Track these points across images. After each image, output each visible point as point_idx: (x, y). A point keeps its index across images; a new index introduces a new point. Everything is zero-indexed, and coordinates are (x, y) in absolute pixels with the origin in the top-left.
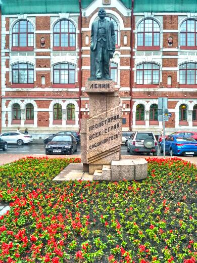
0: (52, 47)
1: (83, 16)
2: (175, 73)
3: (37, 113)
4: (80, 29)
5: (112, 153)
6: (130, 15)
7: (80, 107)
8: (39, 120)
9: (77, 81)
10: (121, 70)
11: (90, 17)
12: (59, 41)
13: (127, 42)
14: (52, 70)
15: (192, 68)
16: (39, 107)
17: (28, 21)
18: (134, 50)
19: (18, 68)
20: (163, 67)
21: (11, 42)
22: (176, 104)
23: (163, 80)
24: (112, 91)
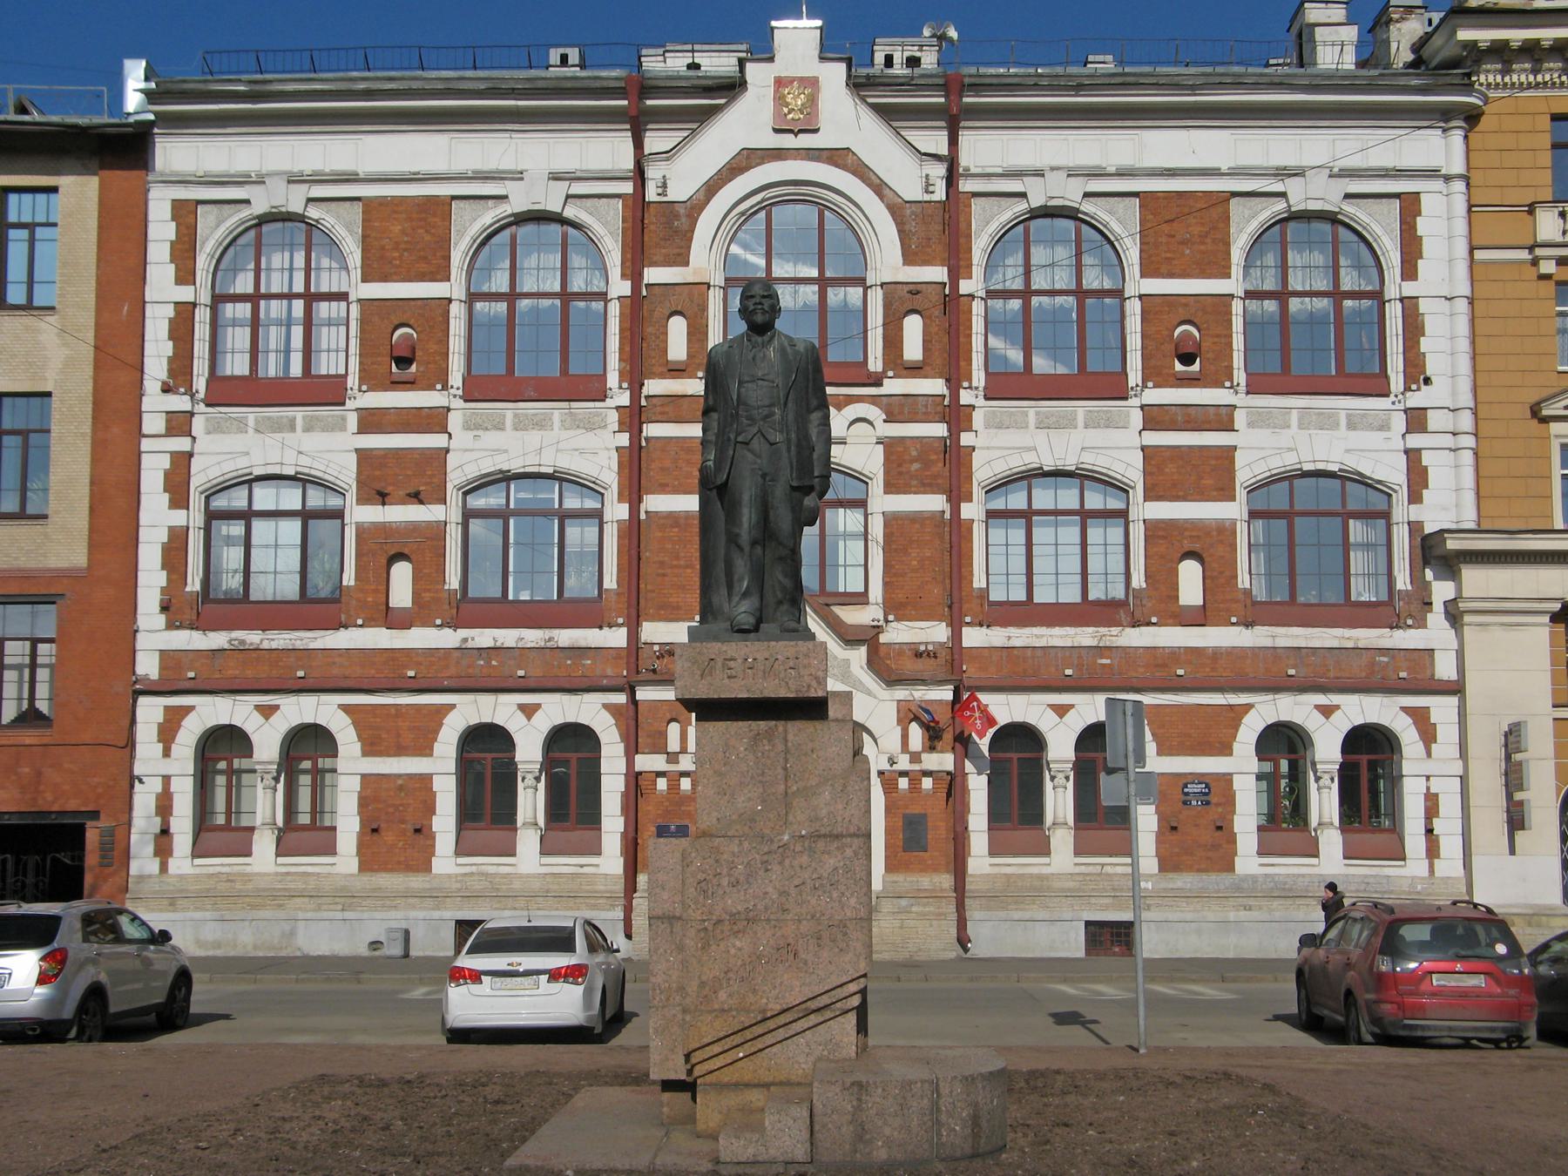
1: (652, 194)
2: (1224, 532)
4: (633, 272)
6: (940, 194)
7: (632, 749)
8: (371, 830)
9: (610, 582)
11: (696, 207)
13: (926, 349)
14: (455, 516)
15: (1323, 507)
16: (371, 747)
18: (966, 397)
19: (1023, 505)
21: (201, 348)
22: (1236, 726)
23: (1148, 576)
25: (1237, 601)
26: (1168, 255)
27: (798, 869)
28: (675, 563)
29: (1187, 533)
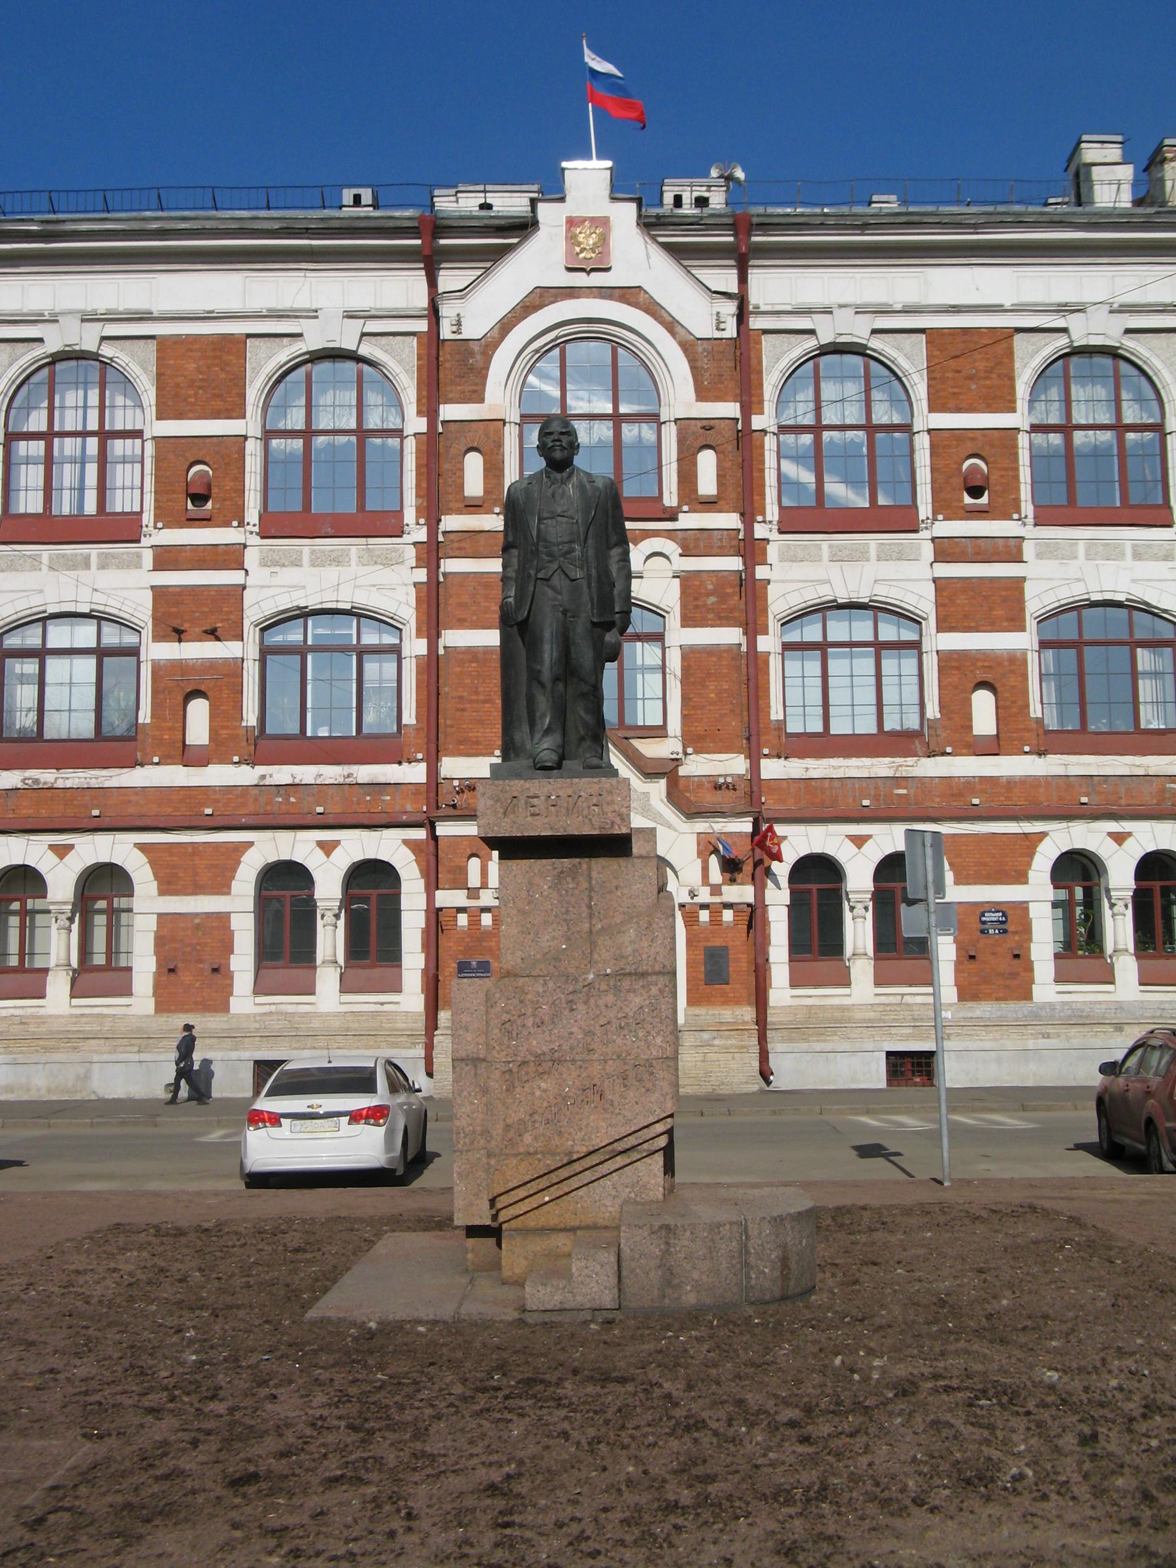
0: (252, 515)
1: (446, 332)
2: (1015, 662)
3: (151, 923)
4: (429, 409)
5: (620, 1161)
7: (433, 884)
8: (167, 970)
10: (690, 655)
12: (299, 483)
16: (168, 885)
17: (106, 365)
18: (760, 531)
19: (818, 638)
20: (940, 629)
22: (1031, 853)
23: (942, 707)
24: (616, 831)
25: (1028, 730)
26: (956, 390)
27: (603, 1008)
28: (474, 697)
29: (980, 664)
